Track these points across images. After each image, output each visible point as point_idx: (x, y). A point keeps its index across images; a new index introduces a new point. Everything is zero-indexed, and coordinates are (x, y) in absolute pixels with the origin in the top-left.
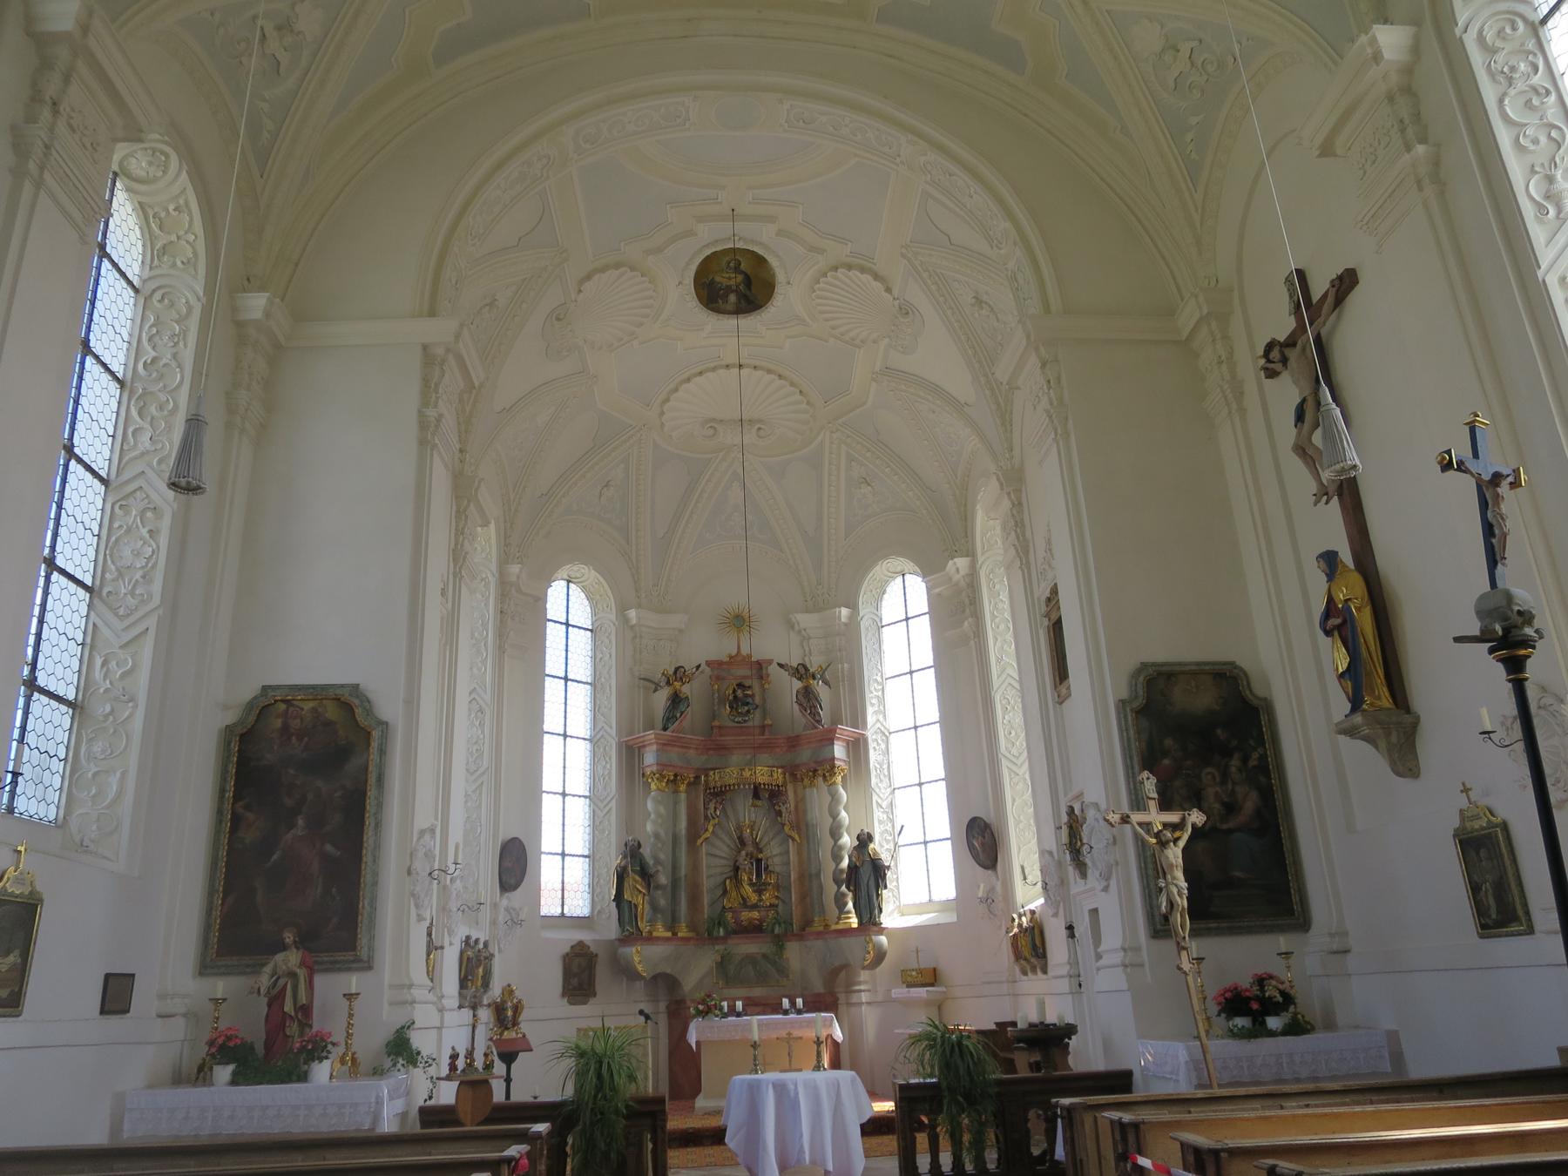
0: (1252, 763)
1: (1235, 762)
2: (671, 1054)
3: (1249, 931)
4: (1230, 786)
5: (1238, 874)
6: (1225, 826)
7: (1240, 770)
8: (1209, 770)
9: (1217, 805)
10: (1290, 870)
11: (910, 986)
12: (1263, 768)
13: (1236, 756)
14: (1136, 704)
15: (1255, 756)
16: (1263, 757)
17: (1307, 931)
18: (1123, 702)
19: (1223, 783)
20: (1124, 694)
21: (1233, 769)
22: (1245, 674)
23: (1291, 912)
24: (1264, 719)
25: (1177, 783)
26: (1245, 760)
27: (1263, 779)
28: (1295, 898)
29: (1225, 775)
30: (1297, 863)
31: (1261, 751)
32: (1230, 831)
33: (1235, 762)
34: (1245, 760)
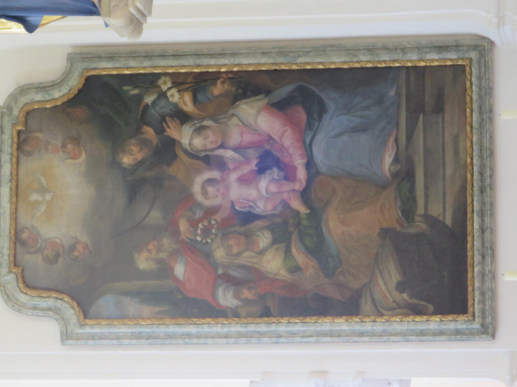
0: (188, 105)
1: (185, 136)
2: (424, 149)
3: (488, 154)
4: (229, 154)
5: (388, 160)
6: (302, 174)
7: (200, 130)
8: (197, 189)
9: (264, 183)
10: (384, 60)
11: (417, 336)
12: (198, 83)
13: (173, 131)
14: (71, 312)
15: (174, 96)
16: (179, 81)
17: (492, 43)
18: (66, 336)
19: (221, 164)
20: (49, 328)
21: (198, 142)
22: (23, 90)
23: (459, 71)
24: (106, 68)
25: (219, 254)
26: (183, 118)
27: (218, 89)
28: (434, 59)
29: (208, 160)
30: (372, 46)
31: (165, 84)
32: (310, 164)
33: (185, 136)
34: (183, 118)
